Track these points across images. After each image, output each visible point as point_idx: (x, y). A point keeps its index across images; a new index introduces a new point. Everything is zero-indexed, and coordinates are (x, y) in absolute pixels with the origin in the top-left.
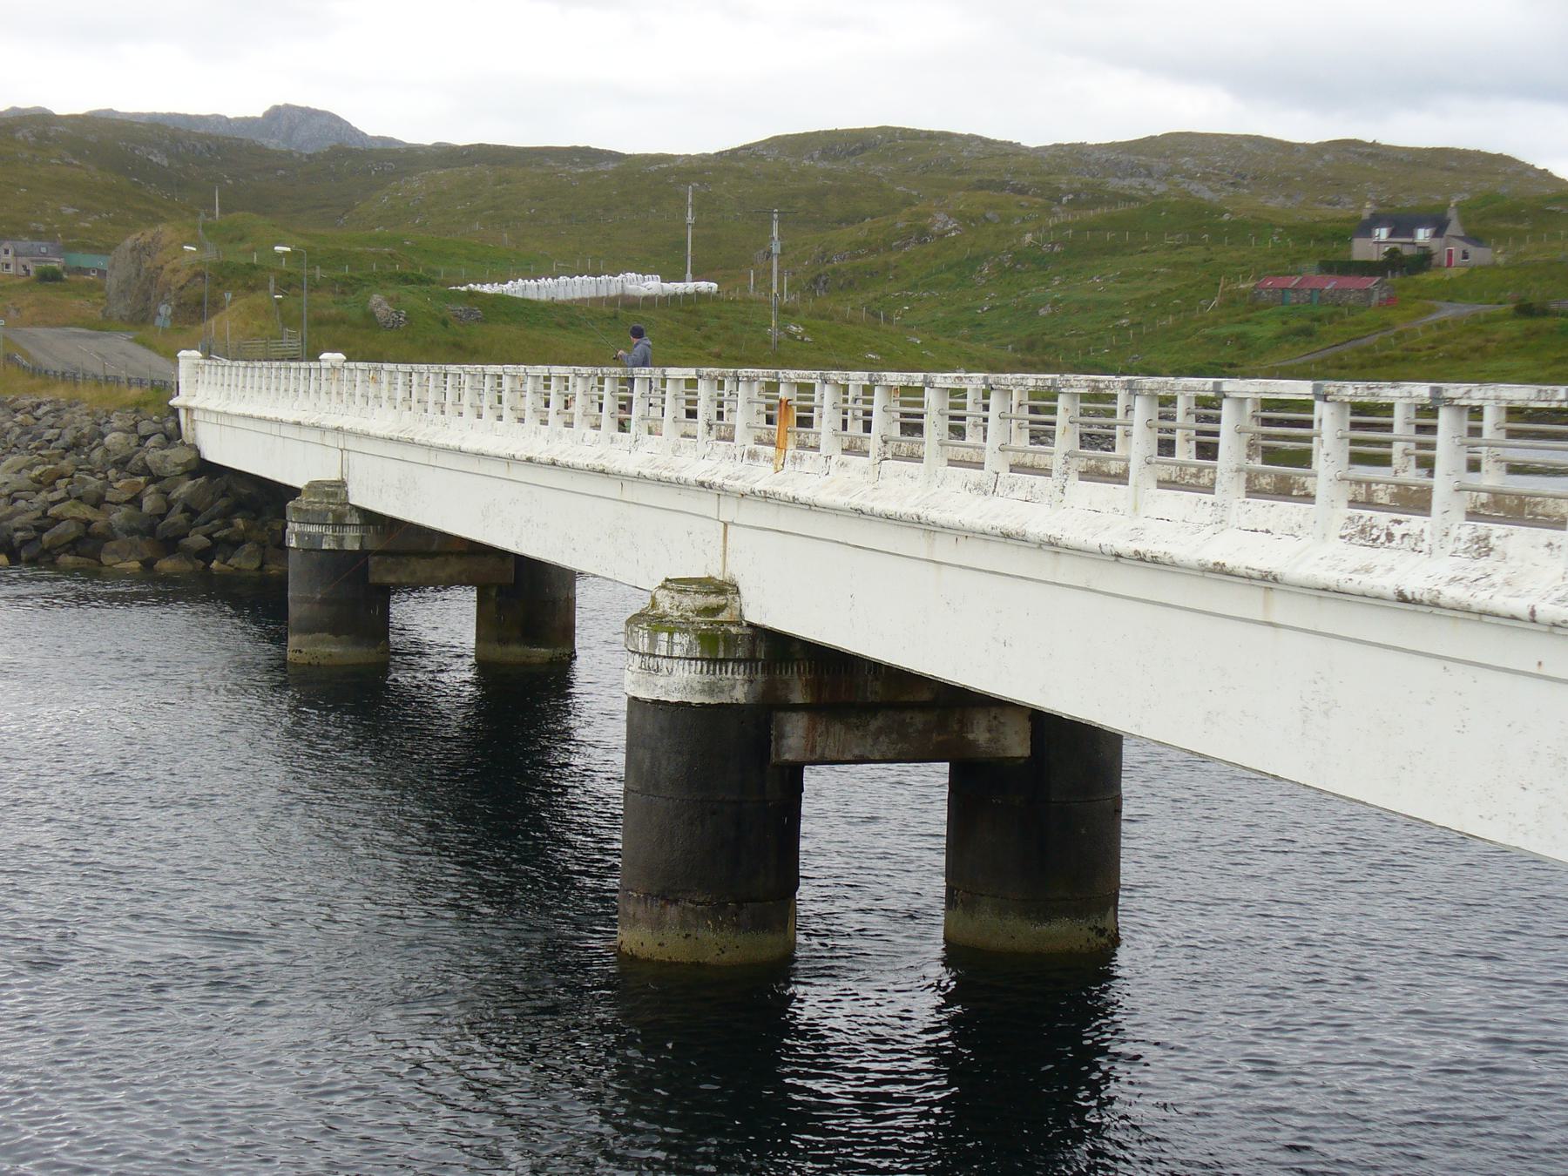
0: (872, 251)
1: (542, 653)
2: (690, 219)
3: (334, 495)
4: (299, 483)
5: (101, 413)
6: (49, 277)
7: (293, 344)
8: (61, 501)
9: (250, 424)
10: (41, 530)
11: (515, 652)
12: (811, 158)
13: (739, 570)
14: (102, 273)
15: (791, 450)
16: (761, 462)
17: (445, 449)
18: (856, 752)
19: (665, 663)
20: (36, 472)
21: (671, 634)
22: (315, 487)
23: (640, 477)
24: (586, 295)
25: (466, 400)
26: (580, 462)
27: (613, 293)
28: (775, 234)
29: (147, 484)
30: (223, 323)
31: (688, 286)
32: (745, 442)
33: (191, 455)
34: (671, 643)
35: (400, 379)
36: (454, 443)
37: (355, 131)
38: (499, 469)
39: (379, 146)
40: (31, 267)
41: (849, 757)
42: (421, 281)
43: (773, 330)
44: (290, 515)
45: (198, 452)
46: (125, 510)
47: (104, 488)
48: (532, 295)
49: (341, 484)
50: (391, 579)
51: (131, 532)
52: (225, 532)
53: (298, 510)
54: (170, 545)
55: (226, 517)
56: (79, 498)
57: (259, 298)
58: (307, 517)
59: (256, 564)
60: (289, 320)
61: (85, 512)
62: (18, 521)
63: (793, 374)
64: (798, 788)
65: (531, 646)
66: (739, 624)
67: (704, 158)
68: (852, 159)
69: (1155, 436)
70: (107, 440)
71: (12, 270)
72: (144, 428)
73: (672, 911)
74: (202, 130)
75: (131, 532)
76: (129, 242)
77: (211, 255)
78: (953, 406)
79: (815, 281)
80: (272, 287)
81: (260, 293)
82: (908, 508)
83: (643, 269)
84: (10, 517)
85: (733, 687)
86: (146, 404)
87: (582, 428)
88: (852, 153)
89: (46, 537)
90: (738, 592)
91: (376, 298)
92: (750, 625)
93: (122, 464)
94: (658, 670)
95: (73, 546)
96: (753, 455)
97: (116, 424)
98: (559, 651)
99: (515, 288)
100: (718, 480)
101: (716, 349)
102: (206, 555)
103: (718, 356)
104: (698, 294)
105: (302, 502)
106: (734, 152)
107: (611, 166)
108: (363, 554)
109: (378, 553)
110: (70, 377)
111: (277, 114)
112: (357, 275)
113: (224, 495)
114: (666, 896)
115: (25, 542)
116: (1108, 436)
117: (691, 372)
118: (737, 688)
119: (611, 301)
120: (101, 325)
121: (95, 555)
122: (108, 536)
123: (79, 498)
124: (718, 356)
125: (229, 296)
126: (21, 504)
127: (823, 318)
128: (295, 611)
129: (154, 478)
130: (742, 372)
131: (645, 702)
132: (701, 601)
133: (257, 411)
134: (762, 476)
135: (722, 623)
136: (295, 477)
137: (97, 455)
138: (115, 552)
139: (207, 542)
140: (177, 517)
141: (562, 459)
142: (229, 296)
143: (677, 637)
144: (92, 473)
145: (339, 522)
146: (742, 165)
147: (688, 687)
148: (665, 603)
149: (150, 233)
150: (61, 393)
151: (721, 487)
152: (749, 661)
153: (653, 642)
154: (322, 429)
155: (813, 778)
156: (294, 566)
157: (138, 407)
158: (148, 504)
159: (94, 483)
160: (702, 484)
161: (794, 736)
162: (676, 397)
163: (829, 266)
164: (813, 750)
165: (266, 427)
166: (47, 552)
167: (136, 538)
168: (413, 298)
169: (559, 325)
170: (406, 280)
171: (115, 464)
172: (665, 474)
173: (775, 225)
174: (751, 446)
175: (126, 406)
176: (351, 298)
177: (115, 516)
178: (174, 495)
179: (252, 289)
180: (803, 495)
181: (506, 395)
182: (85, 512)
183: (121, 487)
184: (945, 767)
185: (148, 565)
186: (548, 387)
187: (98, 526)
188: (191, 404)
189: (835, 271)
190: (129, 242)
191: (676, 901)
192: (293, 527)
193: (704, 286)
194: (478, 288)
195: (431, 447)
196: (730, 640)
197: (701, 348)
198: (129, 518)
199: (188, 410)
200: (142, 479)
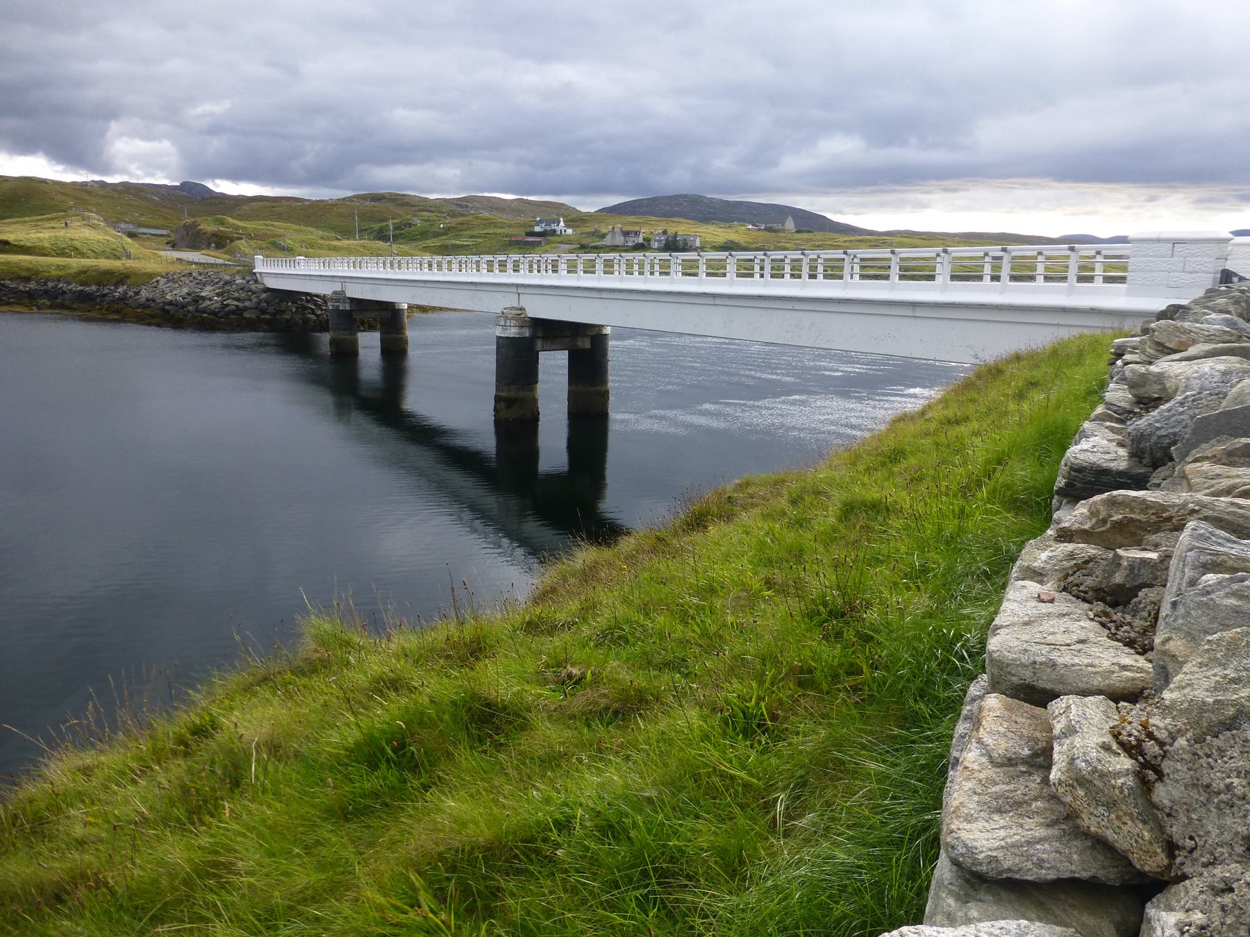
38: (422, 285)
93: (242, 289)
107: (307, 203)
108: (351, 311)
116: (570, 267)
147: (515, 333)
155: (542, 355)
161: (539, 344)
178: (261, 298)
184: (566, 352)
199: (260, 273)
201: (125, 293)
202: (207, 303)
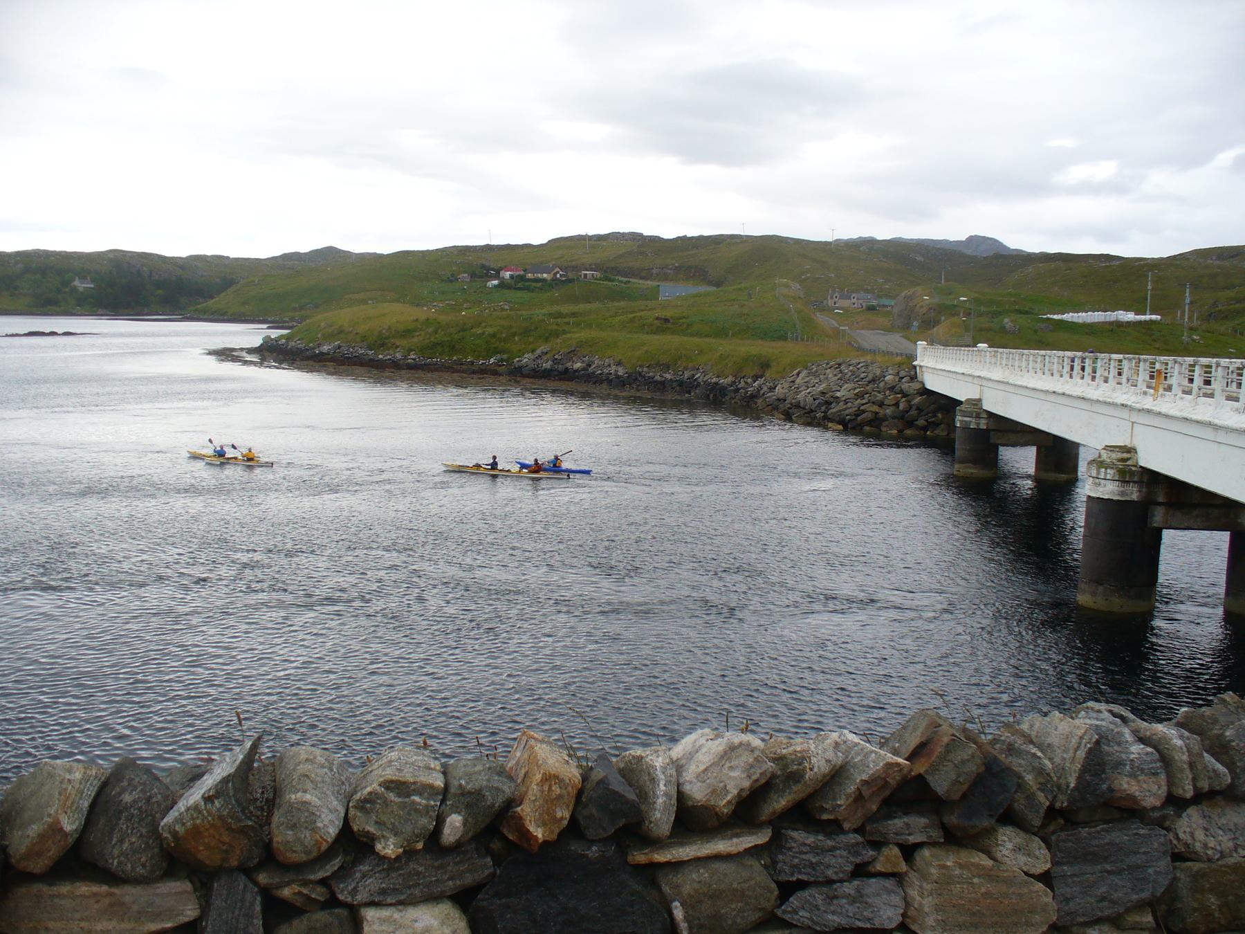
0: (1237, 302)
1: (1064, 477)
2: (1149, 287)
3: (976, 405)
4: (963, 399)
5: (884, 367)
6: (871, 309)
7: (969, 340)
8: (866, 403)
9: (945, 373)
10: (857, 415)
11: (1052, 476)
12: (1211, 259)
13: (1138, 443)
14: (892, 307)
15: (1161, 391)
16: (1148, 396)
17: (1021, 387)
18: (1186, 524)
19: (1103, 481)
20: (856, 391)
21: (1106, 469)
22: (967, 400)
23: (1098, 401)
24: (1100, 320)
25: (1031, 366)
26: (1075, 394)
27: (1112, 320)
28: (1187, 295)
29: (902, 398)
30: (939, 330)
31: (1147, 317)
32: (1142, 386)
33: (921, 386)
34: (1106, 473)
35: (1039, 359)
36: (1024, 384)
37: (1005, 246)
38: (1042, 396)
39: (1015, 253)
40: (864, 304)
41: (1183, 527)
42: (1027, 313)
43: (1185, 338)
44: (958, 412)
45: (924, 384)
46: (892, 408)
47: (884, 398)
48: (1075, 320)
49: (980, 400)
50: (999, 442)
51: (894, 418)
52: (933, 419)
53: (961, 410)
54: (910, 424)
55: (934, 413)
56: (873, 403)
57: (956, 319)
58: (964, 414)
59: (945, 433)
60: (967, 329)
61: (875, 408)
62: (847, 412)
63: (1162, 358)
64: (1159, 538)
65: (1059, 473)
66: (1135, 466)
67: (1162, 259)
68: (1232, 260)
69: (1117, 371)
70: (886, 378)
71: (856, 305)
72: (902, 373)
73: (1101, 589)
74: (938, 246)
75: (894, 418)
76: (903, 294)
77: (936, 300)
78: (1206, 372)
79: (1210, 315)
80: (962, 314)
81: (956, 317)
82: (1206, 418)
83: (1127, 310)
84: (845, 410)
85: (1132, 493)
86: (903, 364)
87: (1077, 379)
88: (1232, 257)
89: (859, 418)
90: (1136, 452)
91: (1006, 320)
92: (1141, 467)
93: (892, 389)
94: (1100, 485)
95: (870, 423)
96: (1145, 393)
97: (891, 372)
98: (1071, 476)
99: (1068, 317)
100: (1129, 403)
101: (1157, 346)
102: (925, 429)
103: (1158, 349)
104: (1151, 320)
105: (963, 407)
106: (1175, 256)
108: (987, 431)
109: (993, 430)
110: (874, 352)
111: (972, 240)
112: (999, 309)
113: (934, 404)
114: (1099, 582)
115: (850, 420)
117: (1120, 356)
118: (1134, 494)
119: (1111, 323)
120: (889, 330)
121: (878, 427)
122: (884, 419)
123: (873, 403)
124: (1158, 349)
125: (943, 318)
126: (850, 404)
127: (1209, 332)
128: (957, 453)
129: (905, 395)
130: (1142, 357)
131: (1093, 498)
132: (1120, 455)
133: (947, 368)
134: (1148, 403)
135: (1128, 465)
136: (961, 397)
137: (882, 385)
138: (887, 426)
139: (926, 423)
140: (913, 412)
141: (1067, 392)
142: (943, 318)
143: (1109, 471)
144: (879, 392)
145: (978, 416)
146: (1178, 262)
147: (1112, 492)
148: (1105, 456)
149: (912, 290)
150: (869, 358)
151: (1130, 407)
152: (1139, 482)
153: (1098, 473)
154: (973, 377)
155: (1167, 535)
156: (958, 435)
157: (900, 365)
158: (902, 406)
159: (880, 397)
160: (1123, 405)
161: (1158, 516)
162: (1115, 367)
163: (1217, 309)
164: (1167, 523)
165: (950, 375)
166: (860, 425)
167: (896, 420)
168: (1022, 320)
169: (1087, 334)
170: (1021, 312)
171: (889, 389)
172: (1109, 400)
173: (1188, 290)
174: (1145, 389)
175: (894, 365)
176: (995, 320)
177: (888, 411)
179: (953, 315)
180: (1164, 411)
181: (1046, 364)
182: (875, 408)
183: (891, 398)
184: (1223, 538)
185: (900, 431)
186: (1063, 361)
187: (881, 415)
188: (922, 364)
189: (1220, 311)
190: (903, 294)
191: (1101, 584)
192: (958, 418)
193: (1154, 317)
194: (1052, 316)
195: (1016, 385)
196: (1132, 473)
197: (1150, 345)
198: (894, 412)
199: (921, 366)
200: (899, 396)
201: (760, 387)
202: (841, 406)
